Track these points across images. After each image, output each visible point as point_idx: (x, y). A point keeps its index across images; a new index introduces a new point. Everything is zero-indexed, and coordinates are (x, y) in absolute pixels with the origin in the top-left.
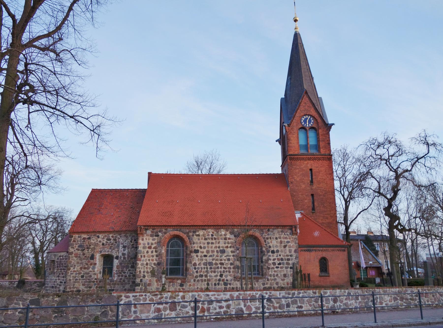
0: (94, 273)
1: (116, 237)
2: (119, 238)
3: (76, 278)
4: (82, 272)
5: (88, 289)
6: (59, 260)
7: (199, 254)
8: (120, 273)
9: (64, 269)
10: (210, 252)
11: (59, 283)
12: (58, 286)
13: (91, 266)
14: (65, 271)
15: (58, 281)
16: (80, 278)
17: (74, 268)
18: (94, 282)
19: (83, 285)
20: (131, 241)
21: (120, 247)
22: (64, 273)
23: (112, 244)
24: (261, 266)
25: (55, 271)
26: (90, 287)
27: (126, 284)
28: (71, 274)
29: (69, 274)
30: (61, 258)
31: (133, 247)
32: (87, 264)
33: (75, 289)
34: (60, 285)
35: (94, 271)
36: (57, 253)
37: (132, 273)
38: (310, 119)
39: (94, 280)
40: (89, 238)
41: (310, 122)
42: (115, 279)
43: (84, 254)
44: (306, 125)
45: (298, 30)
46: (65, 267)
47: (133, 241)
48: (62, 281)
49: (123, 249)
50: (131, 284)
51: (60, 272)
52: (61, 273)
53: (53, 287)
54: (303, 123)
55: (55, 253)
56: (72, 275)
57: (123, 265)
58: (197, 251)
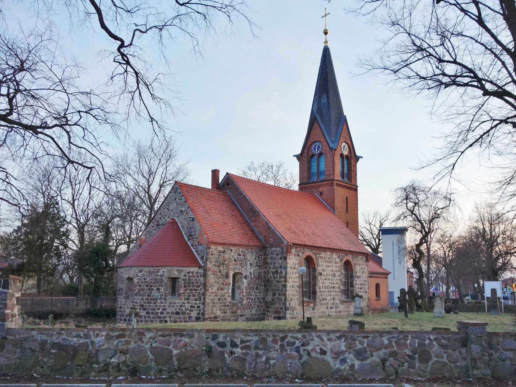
4: (219, 294)
6: (187, 278)
7: (322, 277)
9: (196, 290)
11: (189, 308)
12: (188, 312)
14: (197, 291)
15: (188, 306)
16: (217, 301)
17: (212, 289)
18: (228, 306)
19: (220, 310)
20: (256, 258)
21: (248, 265)
23: (242, 260)
24: (351, 290)
25: (181, 292)
26: (225, 313)
27: (252, 308)
28: (210, 296)
29: (208, 296)
30: (191, 274)
31: (257, 265)
33: (213, 315)
34: (191, 311)
35: (228, 293)
36: (185, 268)
37: (257, 296)
38: (319, 145)
40: (224, 252)
41: (318, 149)
43: (220, 272)
45: (329, 45)
46: (197, 286)
47: (257, 258)
48: (193, 305)
49: (250, 267)
50: (256, 308)
51: (190, 293)
52: (191, 295)
55: (180, 268)
56: (210, 298)
58: (321, 274)
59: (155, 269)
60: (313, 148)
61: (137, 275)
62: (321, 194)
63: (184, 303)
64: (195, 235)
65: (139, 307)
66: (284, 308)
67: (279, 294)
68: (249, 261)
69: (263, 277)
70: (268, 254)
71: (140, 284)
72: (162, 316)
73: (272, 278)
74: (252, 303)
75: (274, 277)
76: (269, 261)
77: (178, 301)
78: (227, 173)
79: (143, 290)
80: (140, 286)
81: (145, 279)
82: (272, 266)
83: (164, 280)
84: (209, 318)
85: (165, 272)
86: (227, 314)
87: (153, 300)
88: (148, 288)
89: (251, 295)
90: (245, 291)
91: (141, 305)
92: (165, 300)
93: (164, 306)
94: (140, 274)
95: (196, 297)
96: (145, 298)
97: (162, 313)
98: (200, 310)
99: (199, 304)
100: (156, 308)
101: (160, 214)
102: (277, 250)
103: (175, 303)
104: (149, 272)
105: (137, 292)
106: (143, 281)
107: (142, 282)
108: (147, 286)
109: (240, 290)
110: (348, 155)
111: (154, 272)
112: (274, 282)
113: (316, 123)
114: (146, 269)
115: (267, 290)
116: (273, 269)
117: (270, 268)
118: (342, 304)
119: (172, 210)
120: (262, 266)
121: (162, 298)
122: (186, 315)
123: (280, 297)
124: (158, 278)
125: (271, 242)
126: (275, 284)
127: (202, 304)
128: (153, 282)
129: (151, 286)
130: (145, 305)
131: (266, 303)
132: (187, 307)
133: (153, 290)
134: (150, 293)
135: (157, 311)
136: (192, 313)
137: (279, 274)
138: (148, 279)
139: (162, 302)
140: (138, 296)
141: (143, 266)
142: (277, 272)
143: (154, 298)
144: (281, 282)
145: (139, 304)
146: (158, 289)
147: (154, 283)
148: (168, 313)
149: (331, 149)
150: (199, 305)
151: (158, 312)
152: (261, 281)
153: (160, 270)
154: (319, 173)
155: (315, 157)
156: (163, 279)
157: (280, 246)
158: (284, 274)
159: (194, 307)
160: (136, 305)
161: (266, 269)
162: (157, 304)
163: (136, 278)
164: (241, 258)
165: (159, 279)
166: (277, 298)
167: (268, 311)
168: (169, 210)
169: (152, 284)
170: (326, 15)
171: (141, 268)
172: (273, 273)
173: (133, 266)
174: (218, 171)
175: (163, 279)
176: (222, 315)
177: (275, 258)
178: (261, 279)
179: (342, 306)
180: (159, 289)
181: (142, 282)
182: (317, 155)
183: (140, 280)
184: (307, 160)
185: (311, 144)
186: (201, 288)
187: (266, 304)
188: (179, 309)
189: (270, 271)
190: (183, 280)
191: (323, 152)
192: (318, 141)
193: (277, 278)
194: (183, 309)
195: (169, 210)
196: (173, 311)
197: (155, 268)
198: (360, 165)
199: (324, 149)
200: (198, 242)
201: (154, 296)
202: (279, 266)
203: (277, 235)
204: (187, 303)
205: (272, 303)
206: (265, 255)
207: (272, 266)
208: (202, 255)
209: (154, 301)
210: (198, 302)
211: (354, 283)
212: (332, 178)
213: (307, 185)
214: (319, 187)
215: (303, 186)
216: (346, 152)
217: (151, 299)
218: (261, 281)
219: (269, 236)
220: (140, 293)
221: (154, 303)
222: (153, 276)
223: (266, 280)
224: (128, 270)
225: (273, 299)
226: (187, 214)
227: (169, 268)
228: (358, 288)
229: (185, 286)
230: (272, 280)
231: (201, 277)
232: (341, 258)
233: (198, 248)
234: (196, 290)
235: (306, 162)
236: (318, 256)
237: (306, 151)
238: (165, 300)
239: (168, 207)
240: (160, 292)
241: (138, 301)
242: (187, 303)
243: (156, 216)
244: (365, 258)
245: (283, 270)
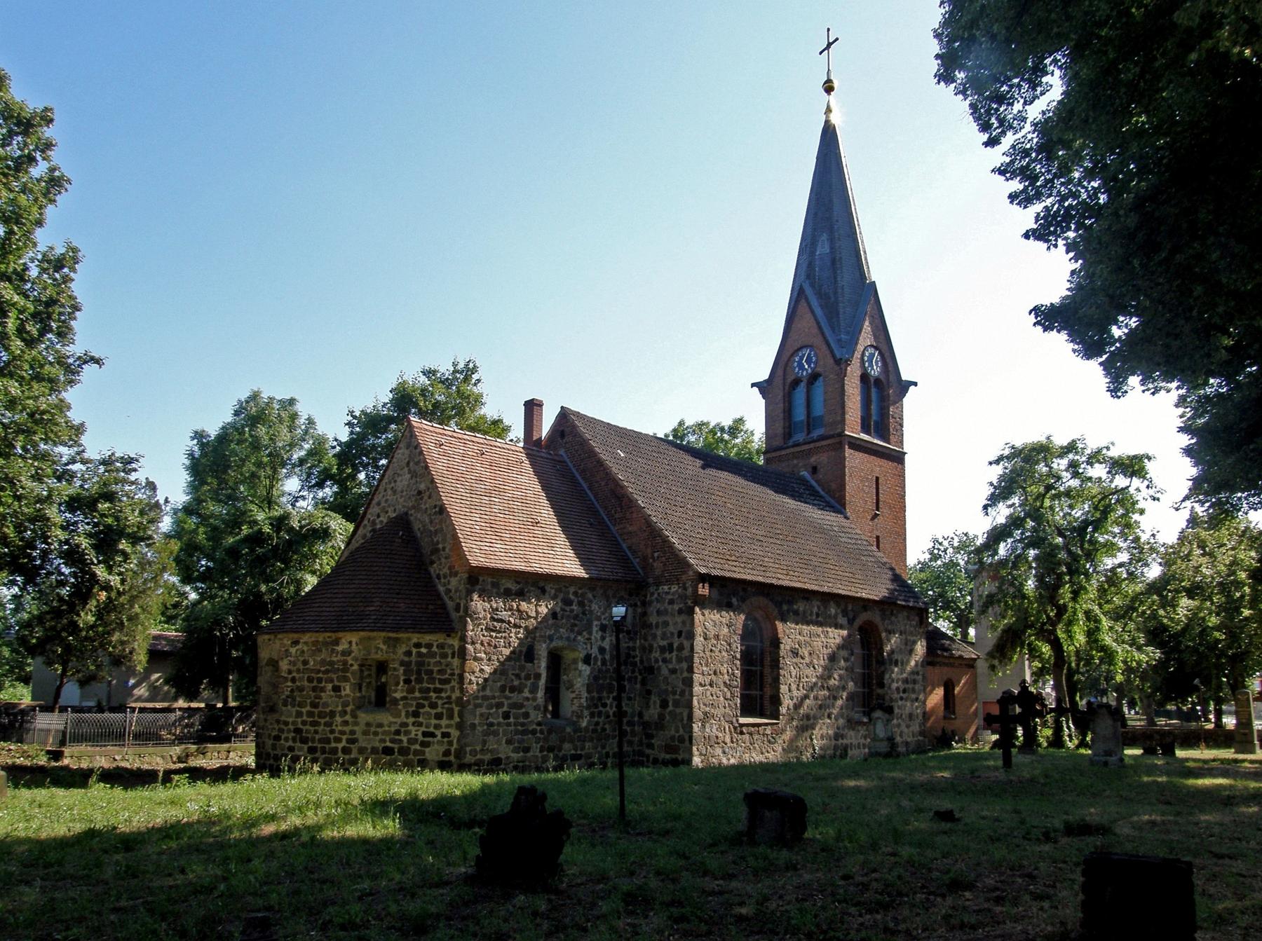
0: (535, 704)
1: (583, 595)
2: (591, 601)
3: (491, 720)
5: (522, 754)
6: (414, 658)
8: (596, 706)
9: (437, 691)
11: (420, 738)
12: (418, 747)
13: (529, 683)
14: (443, 695)
15: (416, 732)
16: (501, 720)
18: (534, 732)
21: (595, 629)
22: (440, 702)
23: (576, 617)
26: (527, 750)
30: (424, 650)
32: (518, 676)
33: (487, 757)
34: (424, 744)
35: (535, 699)
39: (534, 726)
41: (809, 362)
42: (584, 724)
45: (835, 119)
48: (432, 729)
49: (600, 633)
52: (426, 703)
56: (479, 711)
57: (601, 682)
61: (287, 650)
62: (814, 470)
63: (405, 725)
64: (444, 549)
65: (293, 734)
67: (676, 704)
68: (598, 619)
69: (638, 659)
70: (650, 603)
74: (607, 726)
75: (664, 661)
76: (653, 619)
78: (562, 407)
79: (301, 689)
80: (293, 680)
81: (305, 663)
82: (659, 633)
83: (352, 665)
84: (475, 764)
86: (530, 754)
87: (324, 717)
89: (605, 705)
90: (585, 695)
91: (298, 731)
92: (354, 716)
94: (293, 650)
95: (439, 710)
96: (304, 710)
98: (450, 743)
99: (448, 726)
100: (332, 736)
101: (379, 504)
102: (673, 590)
103: (380, 725)
104: (315, 643)
105: (288, 697)
106: (302, 667)
107: (298, 671)
108: (310, 680)
109: (573, 692)
110: (882, 378)
112: (665, 671)
113: (803, 303)
114: (306, 638)
115: (649, 692)
116: (662, 639)
117: (655, 636)
118: (853, 730)
119: (402, 492)
120: (636, 634)
121: (345, 713)
122: (411, 756)
123: (678, 711)
124: (335, 659)
125: (658, 572)
127: (457, 728)
128: (323, 669)
129: (320, 680)
130: (305, 728)
131: (646, 725)
132: (412, 736)
133: (323, 690)
134: (316, 697)
135: (333, 745)
136: (427, 750)
139: (346, 723)
142: (671, 645)
143: (328, 710)
144: (682, 673)
145: (291, 727)
146: (336, 689)
147: (327, 672)
149: (838, 362)
150: (449, 730)
151: (337, 748)
152: (633, 672)
154: (811, 423)
155: (803, 384)
156: (350, 662)
158: (686, 653)
159: (433, 735)
160: (285, 728)
161: (646, 640)
163: (286, 661)
164: (572, 611)
165: (338, 661)
167: (651, 746)
168: (395, 492)
169: (321, 675)
170: (829, 45)
171: (296, 636)
172: (663, 649)
174: (540, 405)
175: (350, 662)
176: (515, 756)
178: (635, 664)
179: (852, 733)
180: (339, 687)
181: (298, 671)
182: (805, 381)
184: (782, 394)
185: (792, 355)
186: (454, 687)
187: (644, 728)
188: (392, 741)
189: (655, 645)
190: (402, 663)
191: (818, 369)
192: (806, 346)
194: (401, 741)
195: (395, 492)
196: (377, 744)
198: (911, 404)
199: (821, 363)
200: (450, 568)
201: (326, 705)
202: (676, 632)
204: (413, 724)
206: (644, 604)
207: (659, 633)
209: (327, 719)
210: (444, 722)
211: (887, 676)
212: (839, 430)
213: (783, 452)
214: (809, 453)
215: (774, 454)
216: (875, 370)
217: (321, 715)
218: (633, 672)
219: (653, 557)
220: (294, 699)
221: (326, 724)
222: (324, 655)
223: (645, 667)
225: (661, 717)
226: (430, 497)
228: (898, 689)
229: (407, 681)
230: (659, 668)
231: (453, 657)
232: (851, 617)
234: (437, 691)
235: (780, 397)
236: (785, 607)
237: (780, 372)
238: (354, 716)
239: (393, 485)
240: (340, 697)
241: (291, 720)
242: (413, 724)
243: (370, 511)
244: (917, 618)
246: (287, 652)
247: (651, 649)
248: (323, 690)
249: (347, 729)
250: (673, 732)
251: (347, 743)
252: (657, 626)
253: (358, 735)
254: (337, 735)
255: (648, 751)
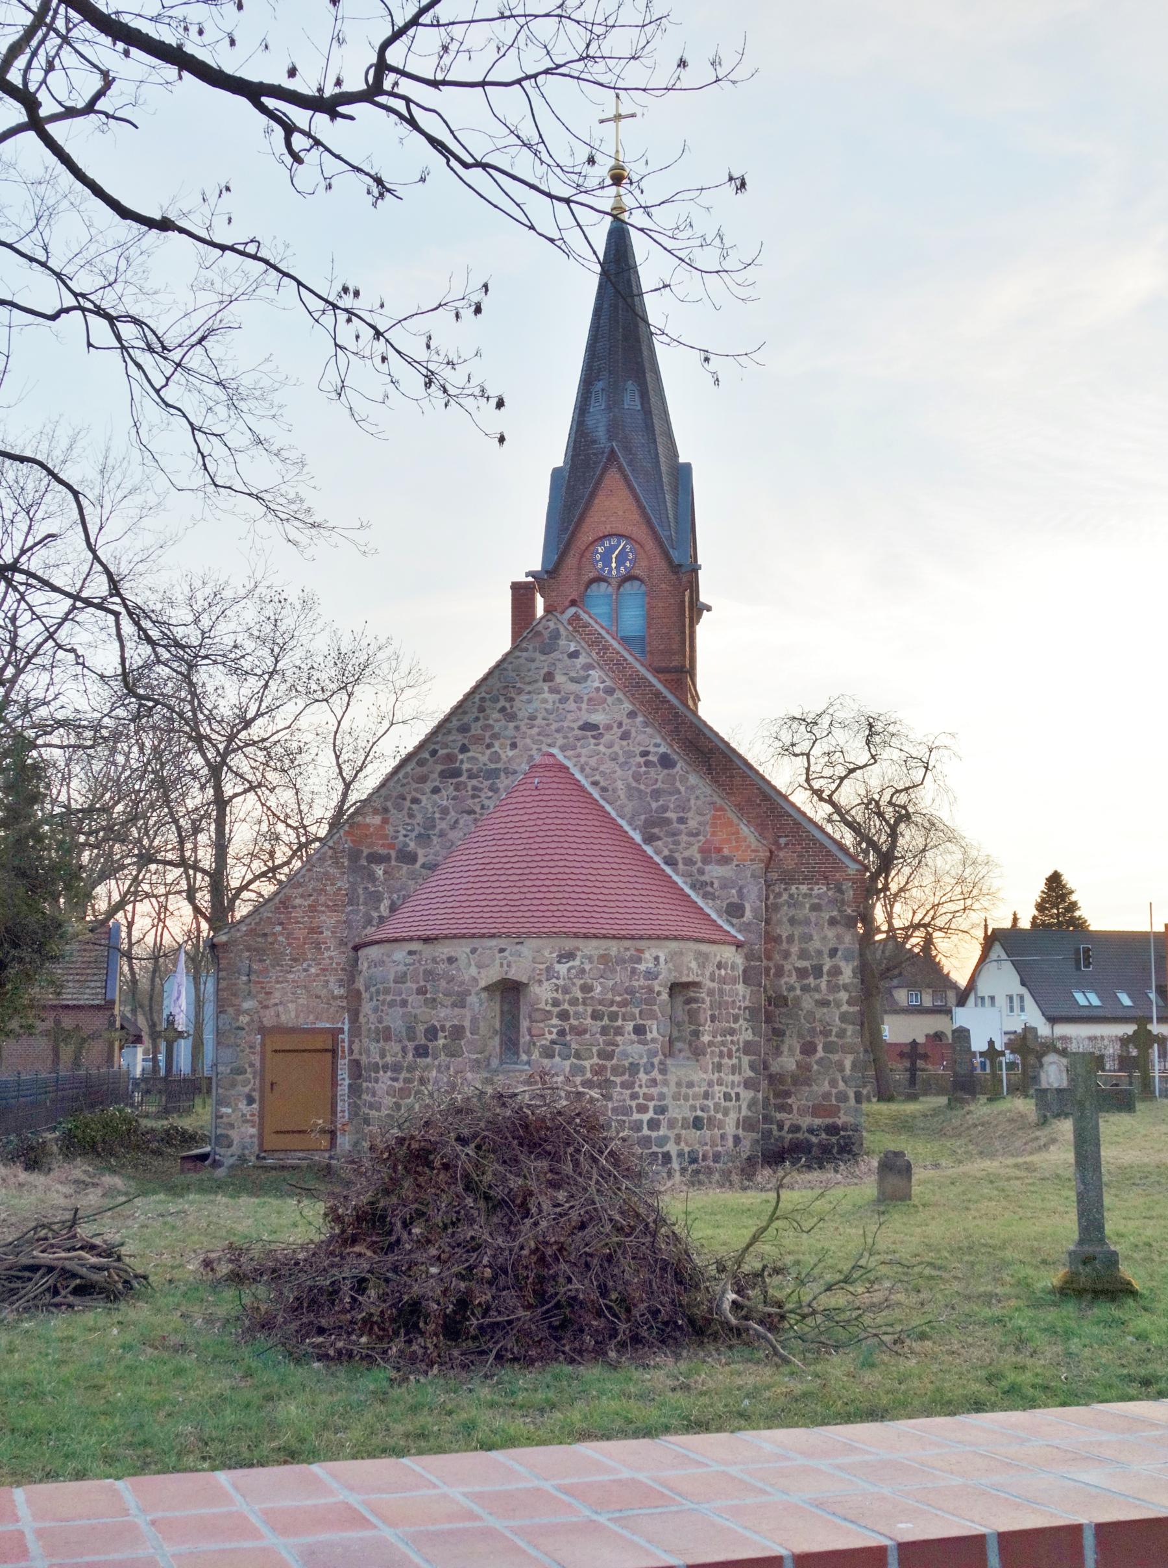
10: (706, 1102)
38: (624, 547)
41: (621, 560)
44: (611, 569)
53: (697, 1123)
54: (600, 565)
55: (704, 947)
59: (627, 949)
60: (598, 557)
61: (548, 969)
64: (682, 820)
66: (852, 1095)
71: (566, 1006)
72: (654, 1134)
73: (798, 992)
75: (805, 989)
76: (784, 931)
77: (700, 1076)
79: (580, 1032)
80: (564, 1016)
82: (795, 949)
83: (659, 994)
85: (662, 960)
87: (623, 1074)
88: (599, 1023)
92: (663, 1071)
93: (662, 1097)
94: (562, 969)
96: (587, 1064)
97: (654, 1124)
102: (816, 892)
103: (690, 1085)
104: (604, 958)
105: (553, 1042)
106: (580, 995)
108: (596, 1016)
111: (621, 961)
112: (807, 1003)
114: (592, 948)
115: (779, 1033)
117: (786, 955)
123: (835, 1057)
124: (636, 984)
126: (811, 1014)
128: (618, 999)
129: (613, 1017)
133: (619, 1031)
135: (636, 1116)
137: (825, 977)
138: (599, 989)
139: (654, 1082)
140: (557, 1059)
141: (576, 936)
142: (818, 971)
143: (626, 1064)
146: (639, 1030)
147: (624, 1004)
148: (672, 1124)
153: (641, 951)
157: (826, 878)
162: (637, 1089)
165: (642, 988)
166: (819, 1062)
169: (614, 1008)
171: (569, 944)
172: (802, 973)
173: (529, 935)
175: (657, 988)
177: (807, 922)
181: (574, 1002)
183: (566, 991)
189: (788, 967)
190: (711, 993)
193: (817, 989)
197: (627, 943)
201: (625, 1055)
202: (826, 952)
203: (815, 840)
205: (803, 1077)
207: (795, 949)
208: (736, 900)
209: (626, 1077)
217: (616, 1070)
221: (624, 1085)
222: (620, 976)
224: (502, 950)
225: (804, 1067)
227: (674, 945)
230: (797, 1000)
233: (701, 872)
238: (663, 1071)
240: (643, 1043)
245: (842, 964)
246: (550, 973)
247: (780, 972)
248: (619, 1031)
249: (654, 1091)
250: (826, 1086)
251: (655, 1113)
252: (790, 939)
253: (668, 1101)
254: (641, 1101)
255: (780, 1116)
